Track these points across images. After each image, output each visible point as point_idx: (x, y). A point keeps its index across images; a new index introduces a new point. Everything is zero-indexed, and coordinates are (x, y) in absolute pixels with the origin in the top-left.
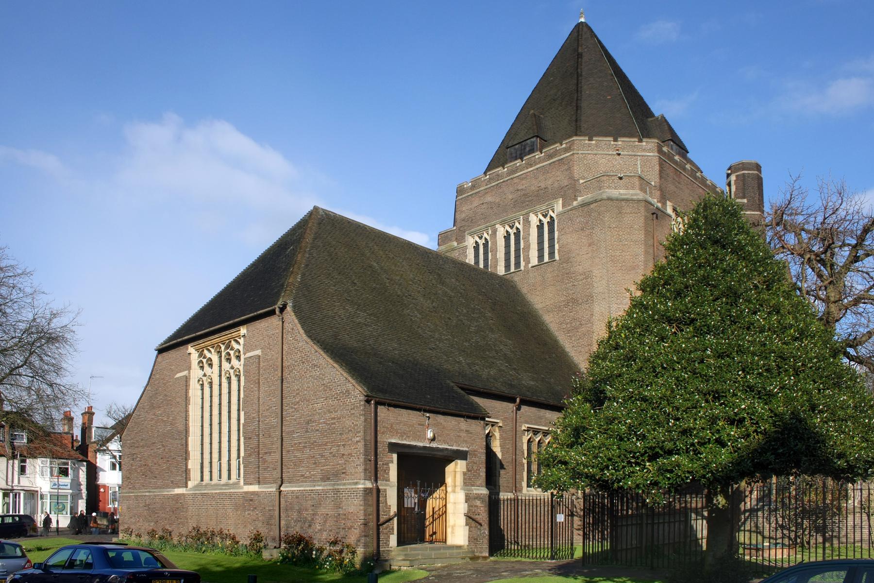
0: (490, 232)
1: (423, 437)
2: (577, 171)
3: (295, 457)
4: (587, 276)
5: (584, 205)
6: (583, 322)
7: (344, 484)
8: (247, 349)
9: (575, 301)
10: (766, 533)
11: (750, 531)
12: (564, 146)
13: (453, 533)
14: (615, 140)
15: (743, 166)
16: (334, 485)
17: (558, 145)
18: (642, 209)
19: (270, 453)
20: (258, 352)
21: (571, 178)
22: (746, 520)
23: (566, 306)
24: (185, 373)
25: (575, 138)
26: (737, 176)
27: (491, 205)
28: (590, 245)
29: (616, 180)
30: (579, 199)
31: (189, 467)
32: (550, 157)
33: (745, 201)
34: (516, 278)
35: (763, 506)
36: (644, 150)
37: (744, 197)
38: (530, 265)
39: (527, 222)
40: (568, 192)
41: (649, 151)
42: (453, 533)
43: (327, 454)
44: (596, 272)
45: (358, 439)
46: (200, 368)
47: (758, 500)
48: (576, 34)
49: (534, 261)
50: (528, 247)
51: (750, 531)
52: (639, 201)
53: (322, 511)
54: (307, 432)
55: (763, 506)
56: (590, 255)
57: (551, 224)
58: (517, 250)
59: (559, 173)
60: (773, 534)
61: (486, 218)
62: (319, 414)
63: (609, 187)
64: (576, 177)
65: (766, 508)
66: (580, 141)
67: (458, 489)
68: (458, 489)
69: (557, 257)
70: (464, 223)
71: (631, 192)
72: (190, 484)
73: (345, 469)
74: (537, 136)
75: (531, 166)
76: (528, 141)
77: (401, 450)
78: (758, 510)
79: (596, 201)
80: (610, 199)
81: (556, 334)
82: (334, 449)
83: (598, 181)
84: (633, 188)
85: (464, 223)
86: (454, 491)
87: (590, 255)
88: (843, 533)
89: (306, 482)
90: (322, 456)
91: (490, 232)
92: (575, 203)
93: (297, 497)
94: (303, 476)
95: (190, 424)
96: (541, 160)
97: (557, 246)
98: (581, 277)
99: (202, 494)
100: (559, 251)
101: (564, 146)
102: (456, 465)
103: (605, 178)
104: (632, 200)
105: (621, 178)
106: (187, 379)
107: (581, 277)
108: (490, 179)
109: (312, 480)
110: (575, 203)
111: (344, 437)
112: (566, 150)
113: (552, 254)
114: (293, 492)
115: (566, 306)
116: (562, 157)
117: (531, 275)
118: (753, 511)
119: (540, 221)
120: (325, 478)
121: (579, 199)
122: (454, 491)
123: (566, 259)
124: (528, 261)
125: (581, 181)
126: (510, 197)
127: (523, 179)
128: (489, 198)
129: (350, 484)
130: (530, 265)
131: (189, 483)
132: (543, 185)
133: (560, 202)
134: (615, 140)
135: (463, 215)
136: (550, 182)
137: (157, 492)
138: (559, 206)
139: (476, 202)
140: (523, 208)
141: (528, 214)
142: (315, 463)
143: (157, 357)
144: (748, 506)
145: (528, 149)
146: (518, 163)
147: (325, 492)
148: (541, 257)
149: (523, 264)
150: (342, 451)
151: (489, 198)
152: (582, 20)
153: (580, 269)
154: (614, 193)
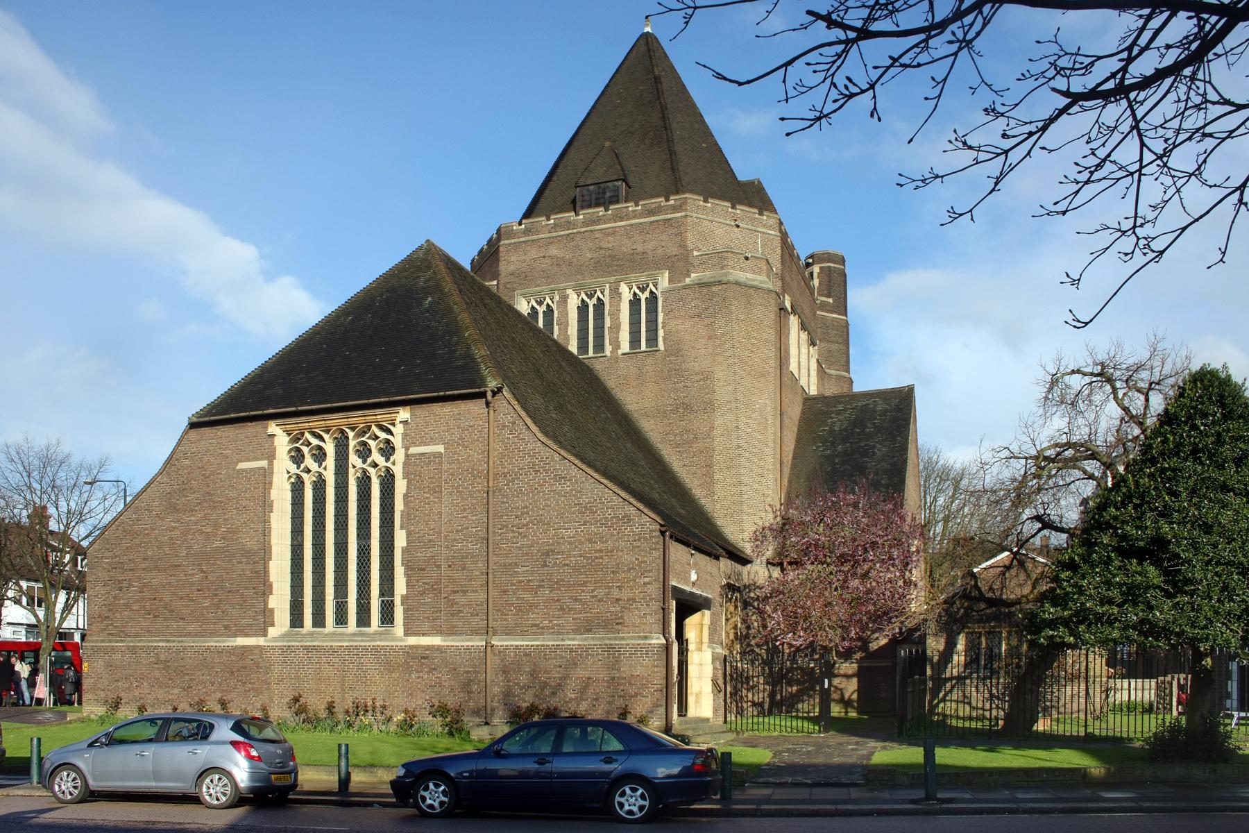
0: (557, 298)
1: (686, 579)
2: (691, 239)
3: (518, 599)
4: (706, 377)
5: (701, 285)
6: (699, 436)
7: (623, 638)
8: (408, 441)
9: (687, 407)
10: (974, 704)
11: (957, 702)
12: (672, 202)
13: (697, 702)
14: (706, 201)
15: (829, 257)
16: (603, 639)
17: (662, 199)
18: (773, 302)
19: (465, 592)
20: (440, 448)
21: (683, 246)
22: (953, 687)
23: (675, 411)
24: (264, 463)
25: (687, 195)
26: (821, 268)
27: (558, 262)
28: (710, 338)
29: (742, 260)
30: (693, 275)
31: (270, 606)
32: (651, 212)
33: (831, 300)
34: (598, 367)
35: (971, 673)
36: (764, 226)
37: (829, 296)
38: (620, 352)
39: (616, 293)
40: (679, 264)
41: (770, 227)
42: (697, 702)
43: (586, 597)
44: (718, 374)
45: (647, 580)
46: (279, 456)
47: (966, 665)
48: (643, 48)
49: (625, 347)
50: (616, 327)
51: (957, 702)
52: (770, 291)
53: (581, 673)
54: (545, 565)
55: (971, 673)
56: (710, 350)
57: (653, 298)
58: (599, 328)
59: (664, 237)
60: (980, 705)
61: (549, 278)
62: (570, 543)
63: (734, 267)
64: (690, 246)
65: (975, 675)
66: (694, 200)
67: (705, 646)
68: (705, 646)
69: (661, 346)
70: (512, 279)
71: (759, 278)
72: (272, 632)
73: (622, 618)
74: (623, 180)
75: (621, 219)
76: (610, 184)
77: (681, 597)
78: (965, 678)
79: (720, 283)
80: (737, 283)
81: (660, 447)
82: (601, 592)
83: (720, 257)
84: (760, 273)
85: (512, 279)
86: (700, 650)
87: (710, 350)
88: (1061, 703)
89: (542, 634)
90: (576, 600)
91: (557, 298)
92: (688, 280)
93: (526, 655)
94: (536, 625)
95: (273, 542)
96: (636, 215)
97: (661, 333)
98: (698, 378)
99: (306, 648)
100: (665, 339)
101: (672, 202)
102: (703, 615)
103: (729, 255)
104: (762, 289)
105: (747, 258)
106: (266, 477)
107: (698, 378)
108: (555, 224)
109: (558, 632)
110: (688, 280)
111: (620, 576)
112: (675, 209)
113: (652, 340)
114: (468, 648)
115: (675, 411)
116: (669, 216)
117: (622, 365)
118: (960, 679)
119: (635, 294)
120: (585, 628)
121: (693, 275)
122: (700, 650)
123: (675, 350)
124: (616, 345)
125: (696, 253)
126: (589, 255)
127: (609, 235)
128: (554, 251)
129: (632, 638)
130: (620, 352)
131: (270, 629)
132: (640, 248)
133: (667, 275)
134: (706, 201)
135: (511, 268)
136: (650, 246)
137: (189, 642)
138: (664, 280)
139: (533, 253)
140: (610, 274)
141: (617, 283)
142: (562, 609)
143: (185, 433)
144: (955, 673)
145: (608, 194)
146: (600, 211)
147: (587, 649)
148: (635, 341)
149: (608, 348)
150: (616, 594)
151: (554, 251)
152: (648, 29)
153: (696, 367)
154: (744, 276)
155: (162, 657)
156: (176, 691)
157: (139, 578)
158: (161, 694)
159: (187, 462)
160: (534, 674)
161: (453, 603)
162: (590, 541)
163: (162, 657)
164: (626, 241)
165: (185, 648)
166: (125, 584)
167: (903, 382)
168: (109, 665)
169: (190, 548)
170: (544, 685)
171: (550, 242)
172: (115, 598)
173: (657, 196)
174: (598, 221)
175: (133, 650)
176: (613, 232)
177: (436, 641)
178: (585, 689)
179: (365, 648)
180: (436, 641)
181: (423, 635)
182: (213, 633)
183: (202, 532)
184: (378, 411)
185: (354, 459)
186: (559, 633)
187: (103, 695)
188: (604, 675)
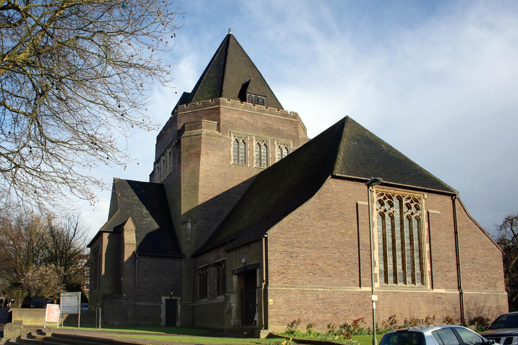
19: (450, 271)
59: (290, 127)
70: (226, 124)
85: (226, 124)
127: (268, 119)
132: (281, 128)
135: (226, 119)
136: (285, 129)
141: (274, 140)
142: (479, 280)
150: (493, 276)
151: (245, 117)
155: (321, 296)
156: (329, 315)
157: (304, 253)
158: (320, 317)
159: (329, 195)
160: (476, 304)
161: (446, 275)
162: (485, 256)
163: (321, 296)
164: (275, 124)
165: (334, 292)
166: (294, 255)
167: (112, 182)
168: (287, 301)
169: (333, 239)
170: (478, 309)
171: (244, 113)
172: (288, 262)
173: (275, 107)
174: (263, 111)
175: (303, 292)
176: (270, 118)
177: (443, 291)
178: (489, 310)
179: (418, 293)
180: (443, 291)
181: (439, 288)
182: (347, 285)
183: (339, 232)
184: (396, 189)
185: (405, 209)
186: (479, 289)
187: (282, 318)
188: (494, 305)
